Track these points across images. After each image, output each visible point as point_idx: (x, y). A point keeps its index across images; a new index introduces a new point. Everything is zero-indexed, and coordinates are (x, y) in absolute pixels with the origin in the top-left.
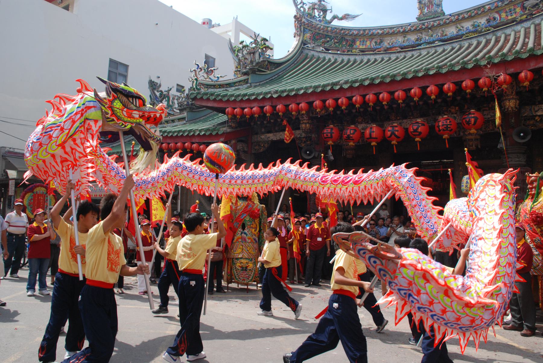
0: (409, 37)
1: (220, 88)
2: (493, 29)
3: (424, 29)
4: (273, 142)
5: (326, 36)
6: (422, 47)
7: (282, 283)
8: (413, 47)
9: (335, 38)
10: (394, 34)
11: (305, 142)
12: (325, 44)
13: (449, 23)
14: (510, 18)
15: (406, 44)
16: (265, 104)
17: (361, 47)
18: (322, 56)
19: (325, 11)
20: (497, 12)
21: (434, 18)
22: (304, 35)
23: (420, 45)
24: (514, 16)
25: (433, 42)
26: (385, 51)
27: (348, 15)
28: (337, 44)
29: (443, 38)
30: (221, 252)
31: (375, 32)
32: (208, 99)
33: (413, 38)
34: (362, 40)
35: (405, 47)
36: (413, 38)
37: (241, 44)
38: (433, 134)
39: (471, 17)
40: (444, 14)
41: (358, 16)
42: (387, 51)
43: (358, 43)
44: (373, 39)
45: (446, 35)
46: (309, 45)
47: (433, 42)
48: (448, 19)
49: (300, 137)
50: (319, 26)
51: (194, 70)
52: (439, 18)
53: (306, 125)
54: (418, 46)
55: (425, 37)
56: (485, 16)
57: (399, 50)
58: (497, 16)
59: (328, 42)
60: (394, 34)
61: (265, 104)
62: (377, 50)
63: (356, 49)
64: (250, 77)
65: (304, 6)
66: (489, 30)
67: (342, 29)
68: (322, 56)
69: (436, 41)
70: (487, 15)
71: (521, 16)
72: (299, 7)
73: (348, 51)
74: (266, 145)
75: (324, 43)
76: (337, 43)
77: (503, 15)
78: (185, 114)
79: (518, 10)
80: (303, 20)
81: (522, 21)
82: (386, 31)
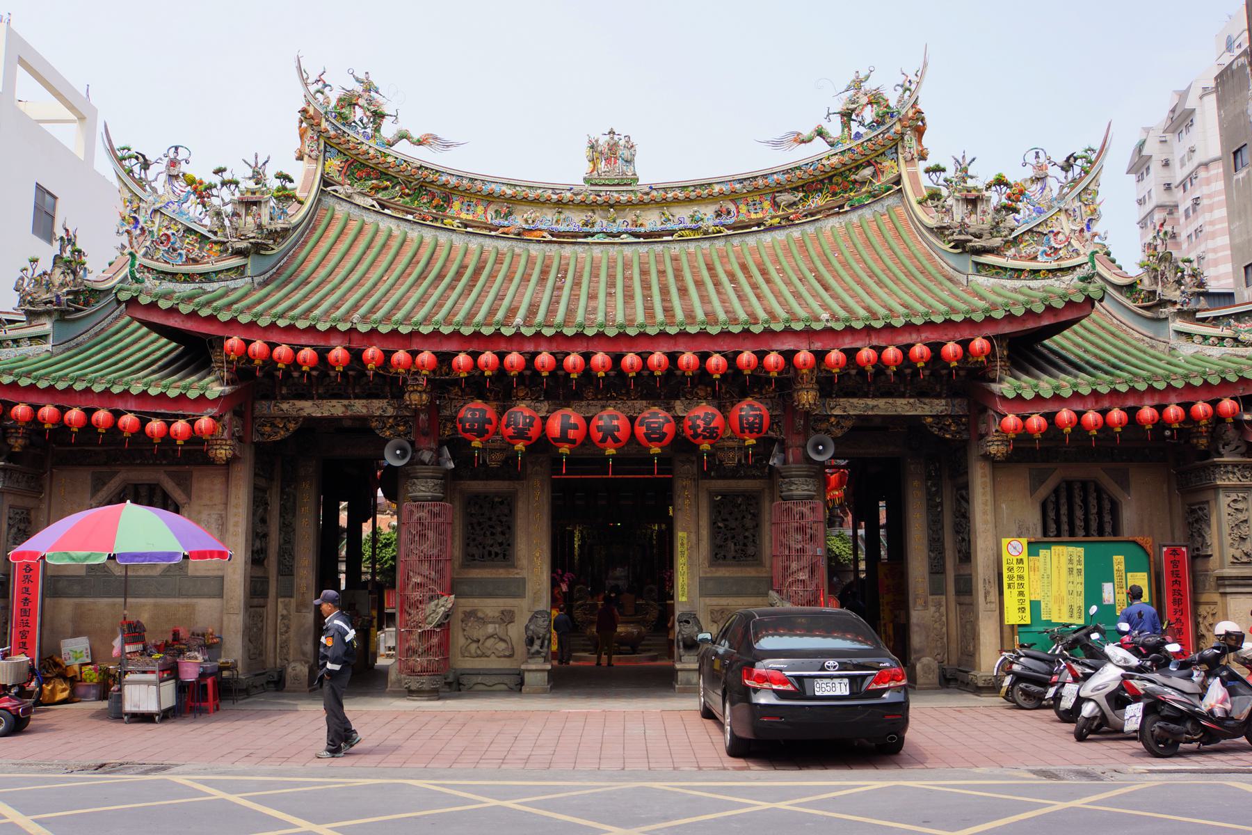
0: (567, 213)
1: (185, 281)
3: (600, 205)
4: (310, 419)
5: (383, 175)
6: (595, 239)
8: (572, 237)
9: (407, 183)
10: (536, 202)
11: (391, 427)
12: (377, 192)
13: (648, 203)
14: (753, 216)
15: (562, 228)
16: (333, 342)
17: (464, 216)
19: (378, 116)
20: (733, 201)
21: (618, 185)
22: (325, 159)
23: (592, 235)
24: (760, 215)
25: (618, 235)
26: (519, 234)
27: (436, 138)
28: (407, 199)
29: (638, 229)
30: (126, 673)
31: (497, 189)
32: (173, 311)
33: (575, 220)
34: (466, 199)
35: (559, 234)
36: (575, 220)
37: (216, 172)
39: (688, 201)
42: (520, 235)
43: (456, 205)
44: (490, 203)
45: (641, 225)
46: (337, 188)
47: (618, 235)
48: (647, 194)
49: (381, 416)
50: (365, 148)
51: (127, 231)
52: (629, 188)
54: (585, 237)
55: (601, 222)
57: (549, 238)
58: (732, 208)
59: (386, 188)
60: (536, 202)
61: (333, 342)
62: (501, 230)
63: (453, 218)
64: (249, 261)
65: (327, 90)
70: (715, 203)
71: (772, 218)
72: (313, 88)
73: (436, 219)
74: (292, 426)
75: (376, 189)
76: (408, 195)
77: (743, 209)
78: (46, 326)
79: (767, 205)
80: (324, 124)
81: (772, 228)
82: (521, 192)
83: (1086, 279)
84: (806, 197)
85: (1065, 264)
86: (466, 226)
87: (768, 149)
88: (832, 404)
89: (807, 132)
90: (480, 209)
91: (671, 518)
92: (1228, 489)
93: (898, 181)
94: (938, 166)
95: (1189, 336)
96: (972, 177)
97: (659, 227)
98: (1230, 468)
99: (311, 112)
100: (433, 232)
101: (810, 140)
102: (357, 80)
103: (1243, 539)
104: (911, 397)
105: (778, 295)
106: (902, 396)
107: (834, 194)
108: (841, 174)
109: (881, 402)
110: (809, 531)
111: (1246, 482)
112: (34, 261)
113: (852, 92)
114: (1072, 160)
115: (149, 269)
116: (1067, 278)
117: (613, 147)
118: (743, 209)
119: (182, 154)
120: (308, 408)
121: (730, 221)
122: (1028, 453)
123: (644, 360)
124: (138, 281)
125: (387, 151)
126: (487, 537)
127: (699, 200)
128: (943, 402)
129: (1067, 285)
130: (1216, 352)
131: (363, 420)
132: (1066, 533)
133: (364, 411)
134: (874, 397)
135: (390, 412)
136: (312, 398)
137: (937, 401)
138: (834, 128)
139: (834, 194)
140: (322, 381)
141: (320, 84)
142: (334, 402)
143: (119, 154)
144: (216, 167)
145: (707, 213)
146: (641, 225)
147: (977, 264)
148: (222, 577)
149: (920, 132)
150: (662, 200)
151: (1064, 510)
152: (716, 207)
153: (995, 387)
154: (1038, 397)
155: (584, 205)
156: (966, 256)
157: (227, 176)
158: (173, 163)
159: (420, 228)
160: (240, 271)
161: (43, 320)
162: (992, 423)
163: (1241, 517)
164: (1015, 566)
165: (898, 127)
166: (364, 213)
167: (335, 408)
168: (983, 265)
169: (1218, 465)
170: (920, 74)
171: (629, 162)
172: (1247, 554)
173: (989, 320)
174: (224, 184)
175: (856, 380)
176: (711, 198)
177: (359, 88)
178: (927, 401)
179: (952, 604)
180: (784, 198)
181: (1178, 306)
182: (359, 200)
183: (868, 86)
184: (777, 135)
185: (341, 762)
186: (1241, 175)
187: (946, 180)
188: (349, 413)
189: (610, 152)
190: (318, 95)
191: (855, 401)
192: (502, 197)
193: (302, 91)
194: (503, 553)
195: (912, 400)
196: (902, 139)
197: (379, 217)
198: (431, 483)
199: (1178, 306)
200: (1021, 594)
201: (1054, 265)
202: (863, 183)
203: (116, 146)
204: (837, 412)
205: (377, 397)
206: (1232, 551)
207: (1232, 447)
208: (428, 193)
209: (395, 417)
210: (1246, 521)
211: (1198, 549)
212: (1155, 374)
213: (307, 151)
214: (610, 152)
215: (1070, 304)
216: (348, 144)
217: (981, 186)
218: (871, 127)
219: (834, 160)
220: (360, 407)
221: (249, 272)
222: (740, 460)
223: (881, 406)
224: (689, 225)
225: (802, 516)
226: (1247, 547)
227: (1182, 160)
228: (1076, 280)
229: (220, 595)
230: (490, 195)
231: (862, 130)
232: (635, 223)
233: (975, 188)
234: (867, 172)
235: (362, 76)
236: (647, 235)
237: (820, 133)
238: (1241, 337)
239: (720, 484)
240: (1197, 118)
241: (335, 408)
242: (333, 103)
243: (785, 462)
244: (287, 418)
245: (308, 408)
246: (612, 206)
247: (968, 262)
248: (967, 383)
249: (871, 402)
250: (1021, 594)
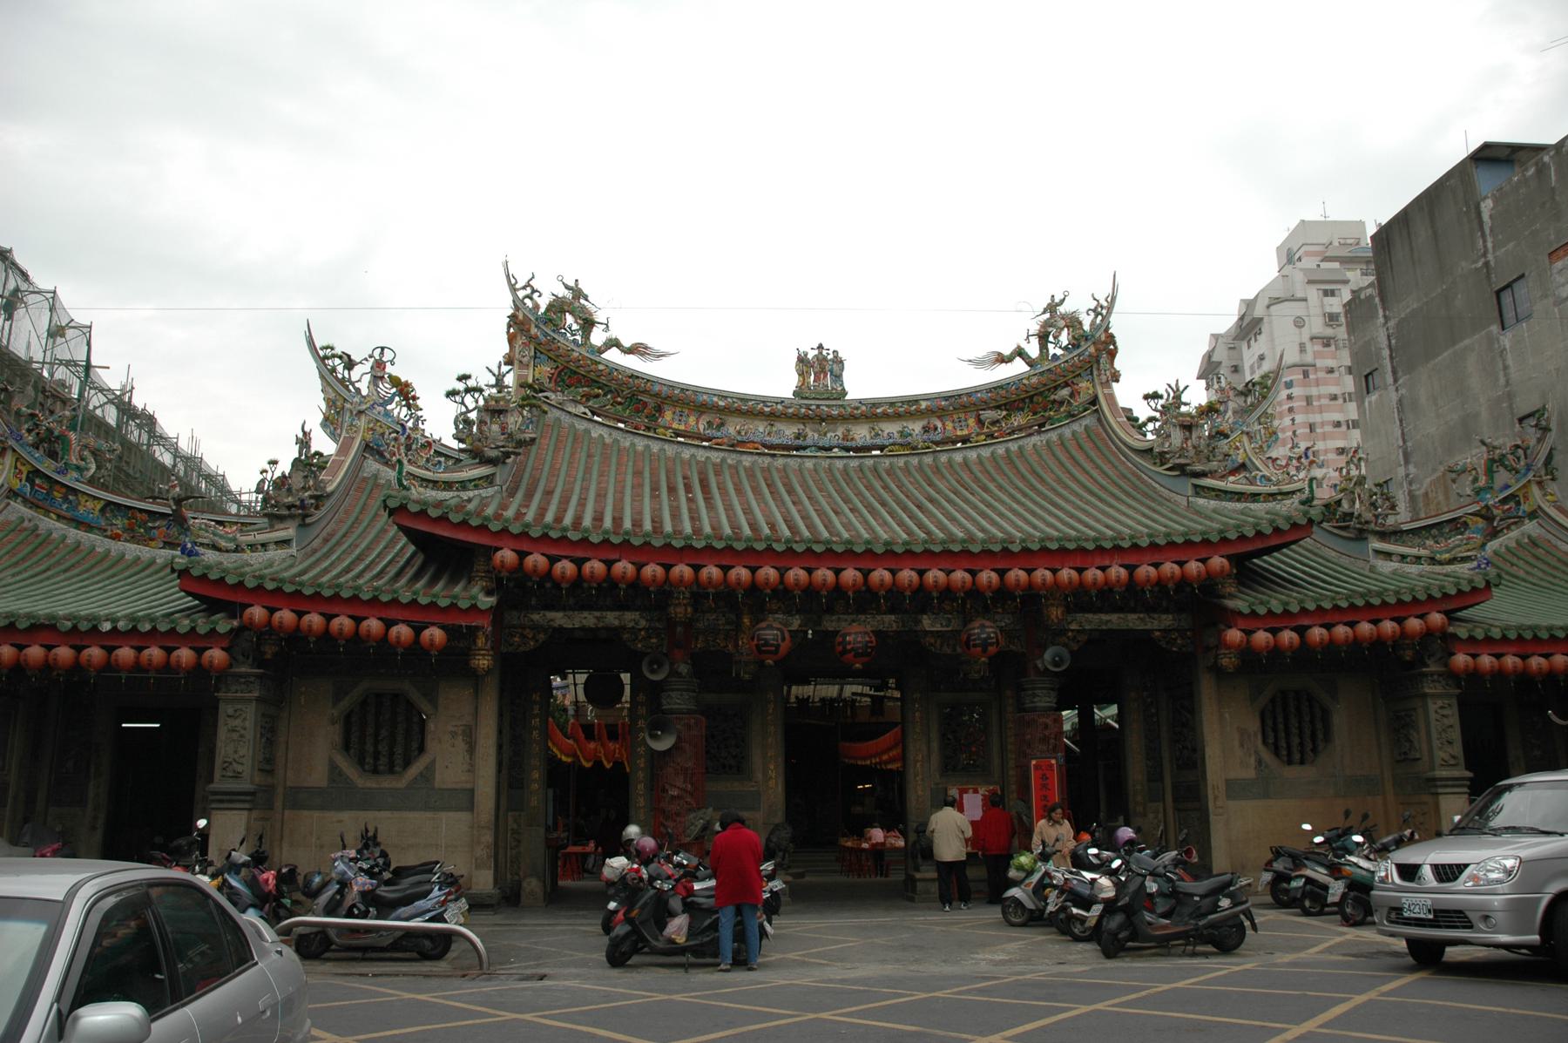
0: (779, 426)
4: (561, 629)
5: (592, 382)
15: (775, 440)
17: (675, 426)
23: (804, 448)
24: (965, 432)
29: (849, 444)
33: (788, 431)
35: (771, 447)
36: (788, 431)
39: (898, 416)
42: (735, 446)
43: (668, 415)
44: (702, 413)
47: (830, 449)
55: (812, 436)
58: (939, 425)
63: (667, 428)
65: (535, 296)
72: (521, 294)
74: (542, 637)
75: (588, 397)
77: (950, 426)
78: (288, 531)
79: (971, 422)
80: (534, 331)
83: (1308, 502)
85: (1286, 488)
86: (678, 435)
89: (1007, 352)
90: (692, 420)
91: (549, 786)
92: (1433, 696)
93: (1094, 401)
95: (1388, 555)
97: (869, 441)
99: (521, 317)
100: (646, 442)
102: (567, 287)
105: (729, 508)
106: (1133, 611)
107: (1035, 414)
108: (1041, 394)
109: (1114, 617)
112: (274, 463)
113: (1047, 315)
115: (415, 477)
116: (1288, 502)
118: (950, 426)
119: (388, 356)
120: (558, 618)
121: (938, 438)
122: (1252, 662)
123: (782, 576)
124: (405, 488)
126: (723, 753)
127: (910, 416)
129: (1289, 507)
130: (1413, 569)
131: (616, 632)
133: (616, 623)
134: (1107, 613)
135: (643, 623)
136: (564, 609)
138: (1033, 350)
139: (1035, 414)
140: (580, 593)
141: (529, 291)
142: (586, 614)
143: (321, 353)
144: (461, 373)
145: (916, 427)
147: (1195, 486)
148: (472, 791)
149: (1112, 354)
150: (873, 412)
151: (1280, 719)
152: (924, 422)
153: (1230, 604)
154: (1286, 613)
155: (796, 418)
156: (1183, 479)
157: (471, 383)
158: (379, 365)
160: (489, 480)
161: (289, 523)
165: (1092, 350)
167: (588, 619)
168: (1203, 488)
169: (1425, 675)
170: (1112, 300)
172: (1454, 757)
173: (1224, 540)
174: (468, 390)
175: (1081, 599)
176: (920, 414)
177: (569, 295)
179: (1170, 812)
180: (989, 415)
183: (1062, 309)
184: (981, 352)
185: (615, 972)
186: (1374, 397)
189: (820, 368)
190: (527, 301)
191: (1090, 616)
192: (715, 408)
193: (510, 298)
194: (738, 766)
196: (1098, 362)
197: (590, 426)
202: (1061, 403)
203: (318, 346)
204: (1073, 627)
205: (628, 609)
206: (1442, 754)
208: (643, 402)
209: (646, 630)
212: (1370, 591)
214: (820, 368)
215: (1295, 526)
216: (554, 349)
218: (1065, 349)
219: (1034, 380)
220: (612, 618)
221: (498, 480)
223: (1114, 620)
225: (1046, 727)
227: (1252, 367)
229: (470, 807)
231: (1059, 352)
232: (845, 438)
234: (1065, 392)
235: (572, 284)
236: (857, 450)
237: (1020, 353)
238: (1438, 557)
240: (1265, 328)
241: (588, 619)
242: (542, 310)
244: (536, 628)
245: (558, 618)
247: (1187, 485)
248: (1199, 603)
249: (1105, 617)
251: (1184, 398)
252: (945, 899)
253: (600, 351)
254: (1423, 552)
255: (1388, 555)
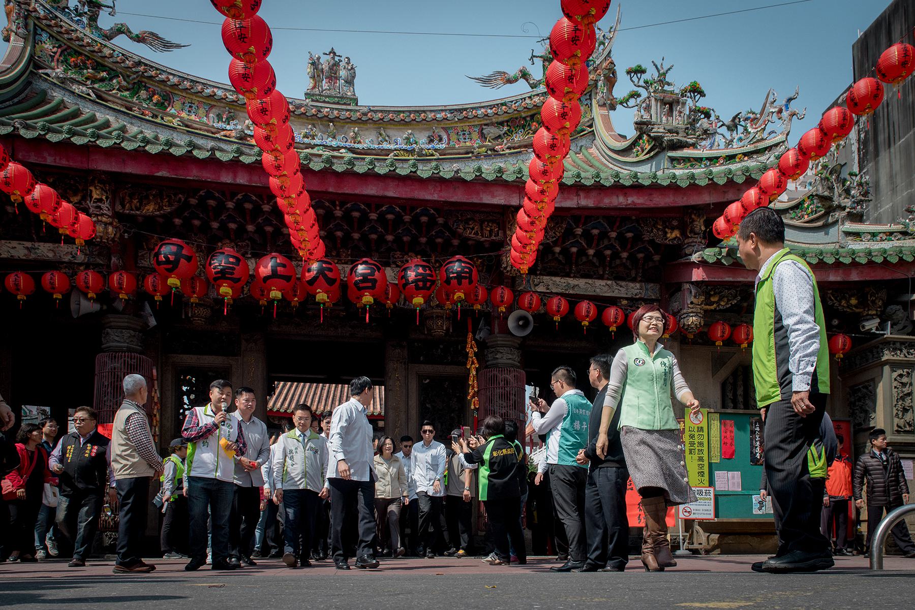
2: (437, 156)
7: (483, 496)
12: (93, 82)
18: (87, 110)
20: (445, 129)
28: (126, 93)
29: (356, 146)
38: (710, 176)
39: (404, 123)
40: (356, 101)
41: (178, 46)
44: (213, 106)
46: (49, 71)
49: (70, 263)
53: (106, 228)
56: (425, 129)
58: (445, 137)
59: (102, 80)
66: (432, 155)
67: (139, 63)
68: (87, 110)
69: (343, 147)
71: (479, 147)
84: (508, 133)
87: (479, 85)
88: (536, 281)
89: (512, 72)
94: (640, 66)
95: (857, 235)
96: (669, 84)
98: (898, 345)
101: (516, 80)
103: (905, 410)
104: (608, 279)
106: (601, 278)
109: (581, 282)
110: (512, 397)
111: (911, 358)
114: (737, 121)
117: (334, 67)
118: (454, 137)
125: (107, 43)
128: (638, 285)
132: (742, 406)
133: (51, 255)
134: (575, 277)
137: (631, 285)
142: (14, 243)
146: (359, 142)
147: (672, 159)
159: (139, 123)
162: (687, 294)
163: (906, 390)
164: (696, 434)
166: (79, 101)
171: (350, 82)
178: (623, 283)
180: (492, 131)
181: (848, 210)
182: (75, 88)
184: (486, 72)
187: (646, 82)
188: (33, 256)
191: (557, 279)
195: (609, 282)
198: (126, 334)
199: (848, 210)
200: (701, 459)
201: (750, 148)
207: (900, 326)
210: (909, 394)
211: (860, 424)
213: (14, 28)
217: (677, 91)
222: (448, 329)
224: (404, 147)
225: (507, 382)
226: (909, 417)
228: (772, 158)
230: (212, 96)
233: (672, 92)
237: (525, 75)
239: (428, 369)
243: (491, 332)
246: (331, 120)
249: (572, 281)
250: (701, 459)
251: (668, 78)
252: (411, 551)
253: (109, 37)
254: (894, 228)
255: (857, 235)
